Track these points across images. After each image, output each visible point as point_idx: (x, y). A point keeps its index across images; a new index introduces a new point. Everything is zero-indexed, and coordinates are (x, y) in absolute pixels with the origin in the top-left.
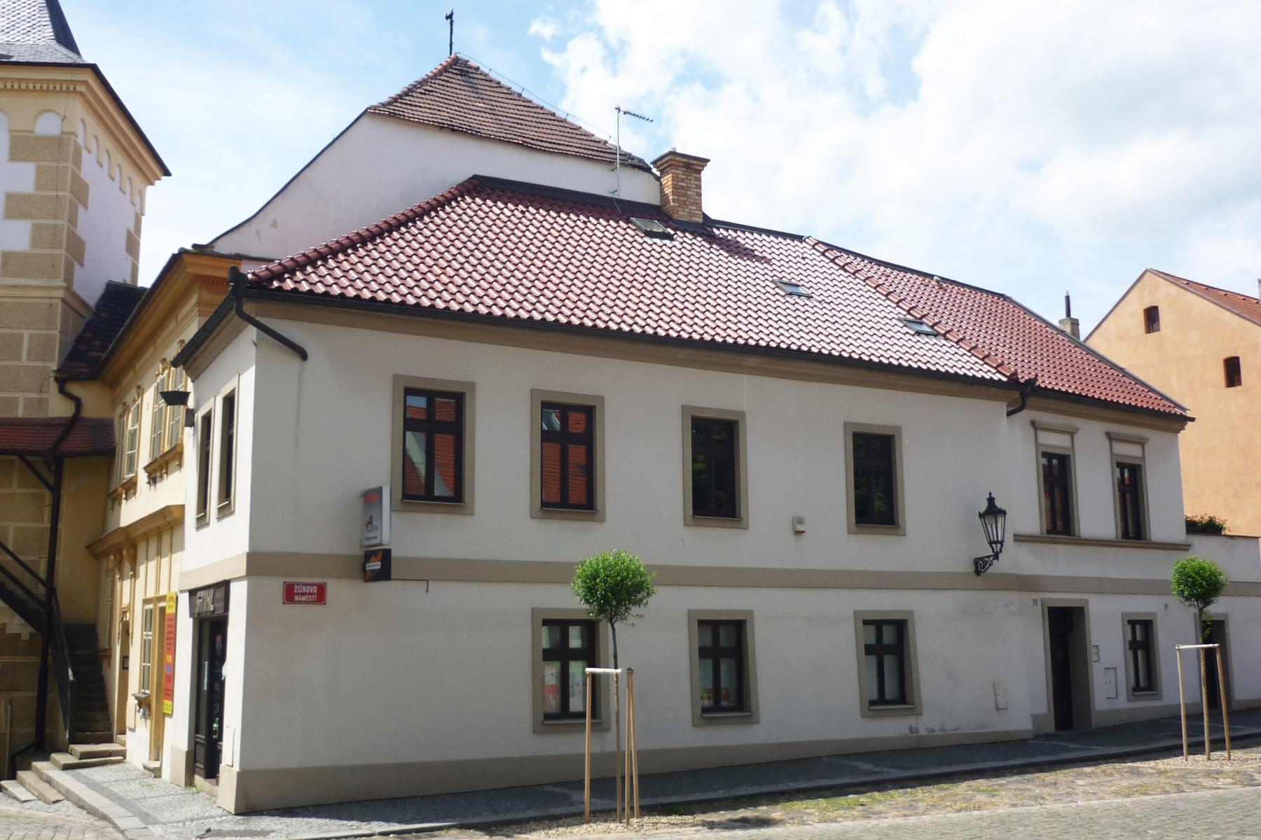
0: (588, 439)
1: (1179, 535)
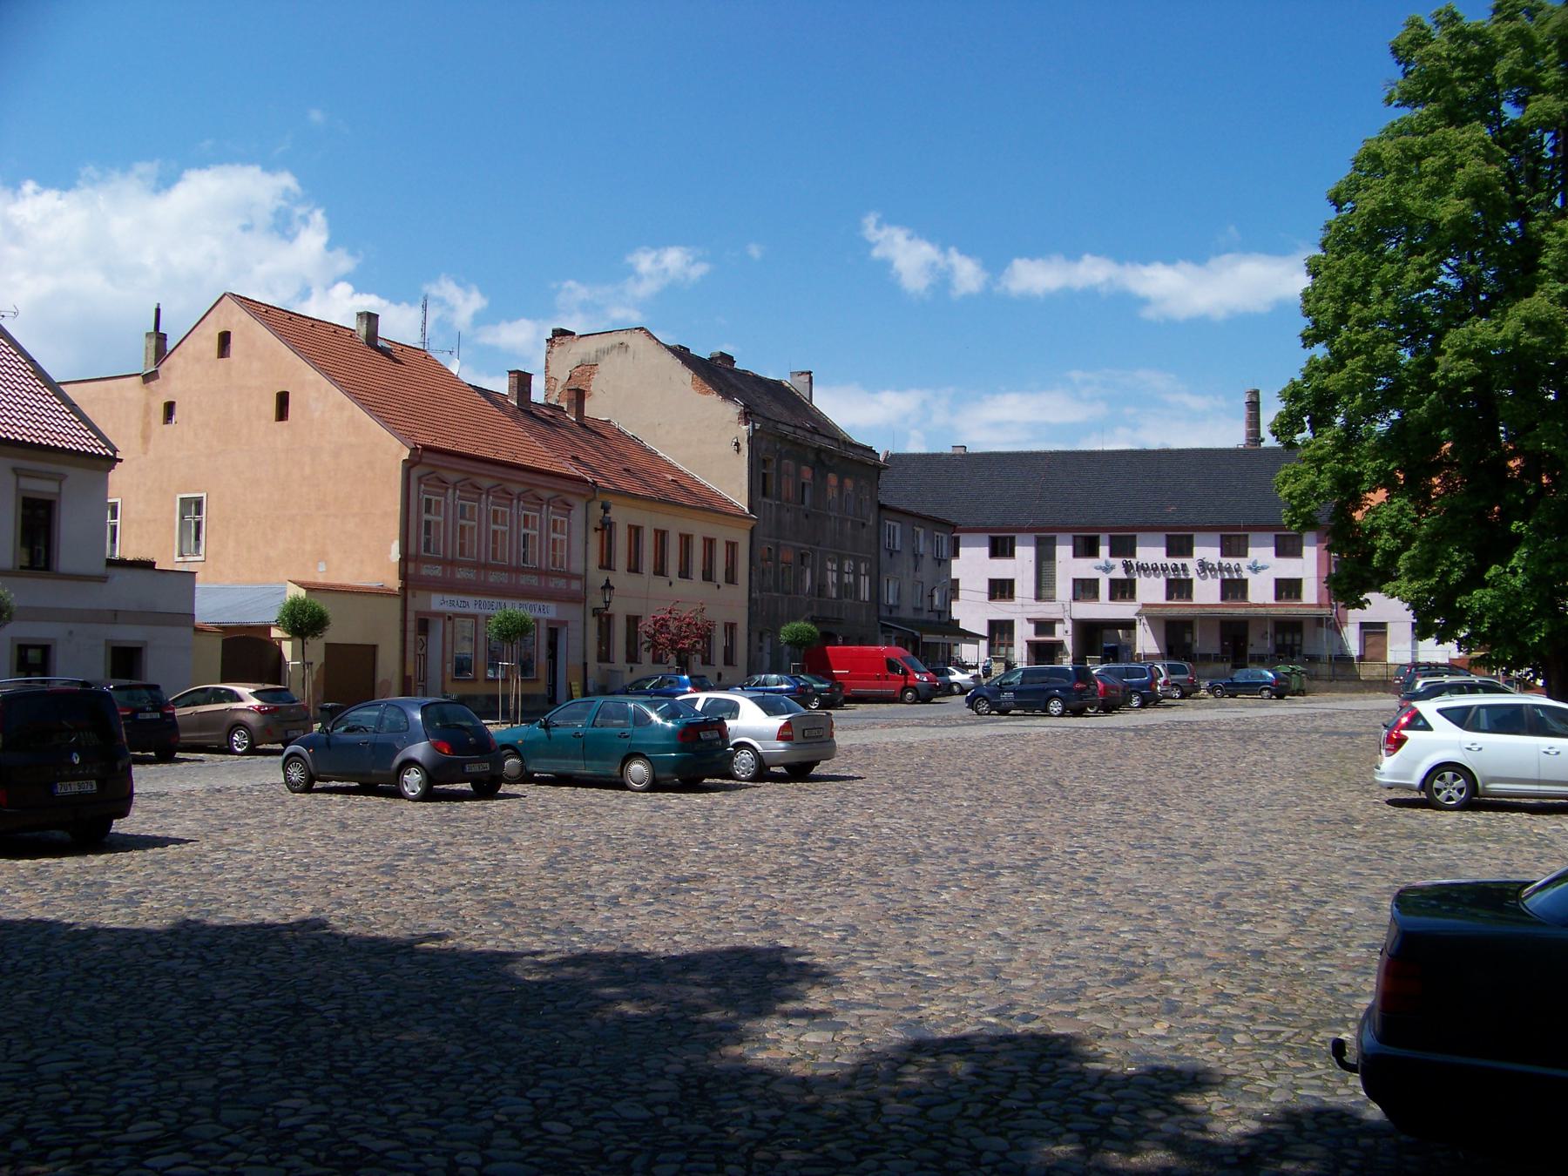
0: (556, 635)
1: (101, 568)
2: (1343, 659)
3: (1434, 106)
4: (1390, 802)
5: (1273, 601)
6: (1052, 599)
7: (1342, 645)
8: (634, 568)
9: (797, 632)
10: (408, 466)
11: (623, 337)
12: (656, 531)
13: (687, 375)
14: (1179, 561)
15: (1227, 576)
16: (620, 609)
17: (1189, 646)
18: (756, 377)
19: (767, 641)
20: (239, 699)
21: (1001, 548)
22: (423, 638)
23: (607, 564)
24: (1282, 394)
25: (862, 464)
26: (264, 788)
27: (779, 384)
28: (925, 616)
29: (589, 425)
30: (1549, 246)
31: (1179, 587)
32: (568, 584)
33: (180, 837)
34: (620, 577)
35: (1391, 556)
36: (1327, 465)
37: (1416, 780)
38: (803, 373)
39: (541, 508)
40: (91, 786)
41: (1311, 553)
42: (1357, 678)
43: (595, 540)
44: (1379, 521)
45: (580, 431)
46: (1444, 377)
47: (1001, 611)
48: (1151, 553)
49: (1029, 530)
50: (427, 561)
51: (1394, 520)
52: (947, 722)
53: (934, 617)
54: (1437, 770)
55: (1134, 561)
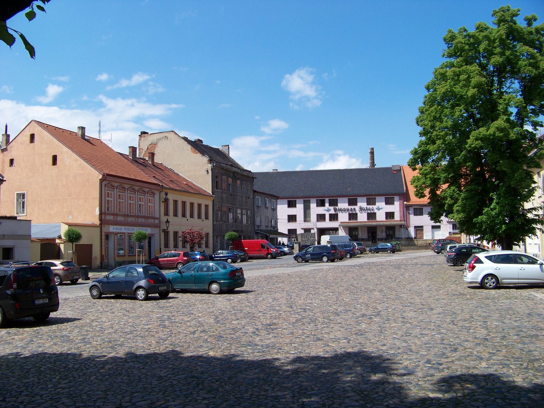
2: (409, 239)
3: (461, 58)
4: (469, 287)
5: (385, 220)
6: (309, 221)
7: (409, 233)
8: (175, 215)
9: (231, 236)
10: (102, 181)
11: (166, 134)
12: (198, 204)
13: (189, 147)
14: (353, 207)
15: (369, 212)
16: (171, 230)
17: (357, 236)
18: (210, 147)
19: (219, 239)
20: (56, 266)
21: (292, 204)
22: (107, 241)
23: (167, 214)
24: (411, 152)
25: (248, 177)
26: (83, 298)
27: (218, 149)
28: (269, 228)
29: (156, 165)
30: (500, 104)
31: (353, 216)
32: (154, 221)
33: (73, 317)
34: (171, 218)
35: (451, 206)
36: (429, 176)
37: (479, 280)
38: (226, 146)
39: (125, 192)
40: (46, 301)
41: (397, 204)
42: (414, 245)
43: (162, 205)
44: (446, 194)
45: (153, 167)
46: (470, 146)
47: (292, 226)
48: (343, 205)
49: (301, 198)
50: (109, 214)
51: (451, 194)
52: (288, 266)
53: (272, 229)
54: (486, 276)
55: (337, 208)
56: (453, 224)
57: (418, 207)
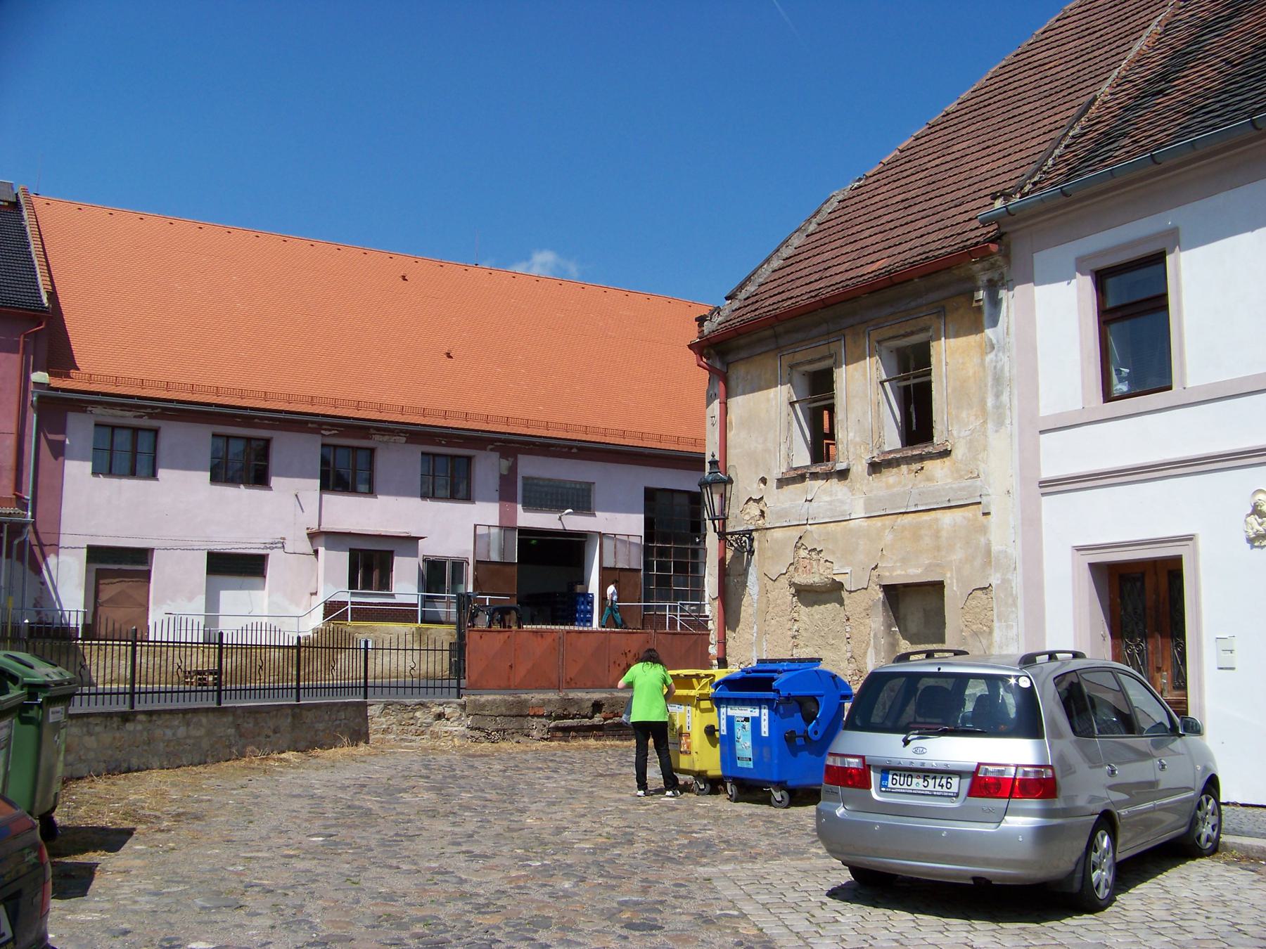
7: (43, 596)
56: (354, 555)
57: (129, 418)
